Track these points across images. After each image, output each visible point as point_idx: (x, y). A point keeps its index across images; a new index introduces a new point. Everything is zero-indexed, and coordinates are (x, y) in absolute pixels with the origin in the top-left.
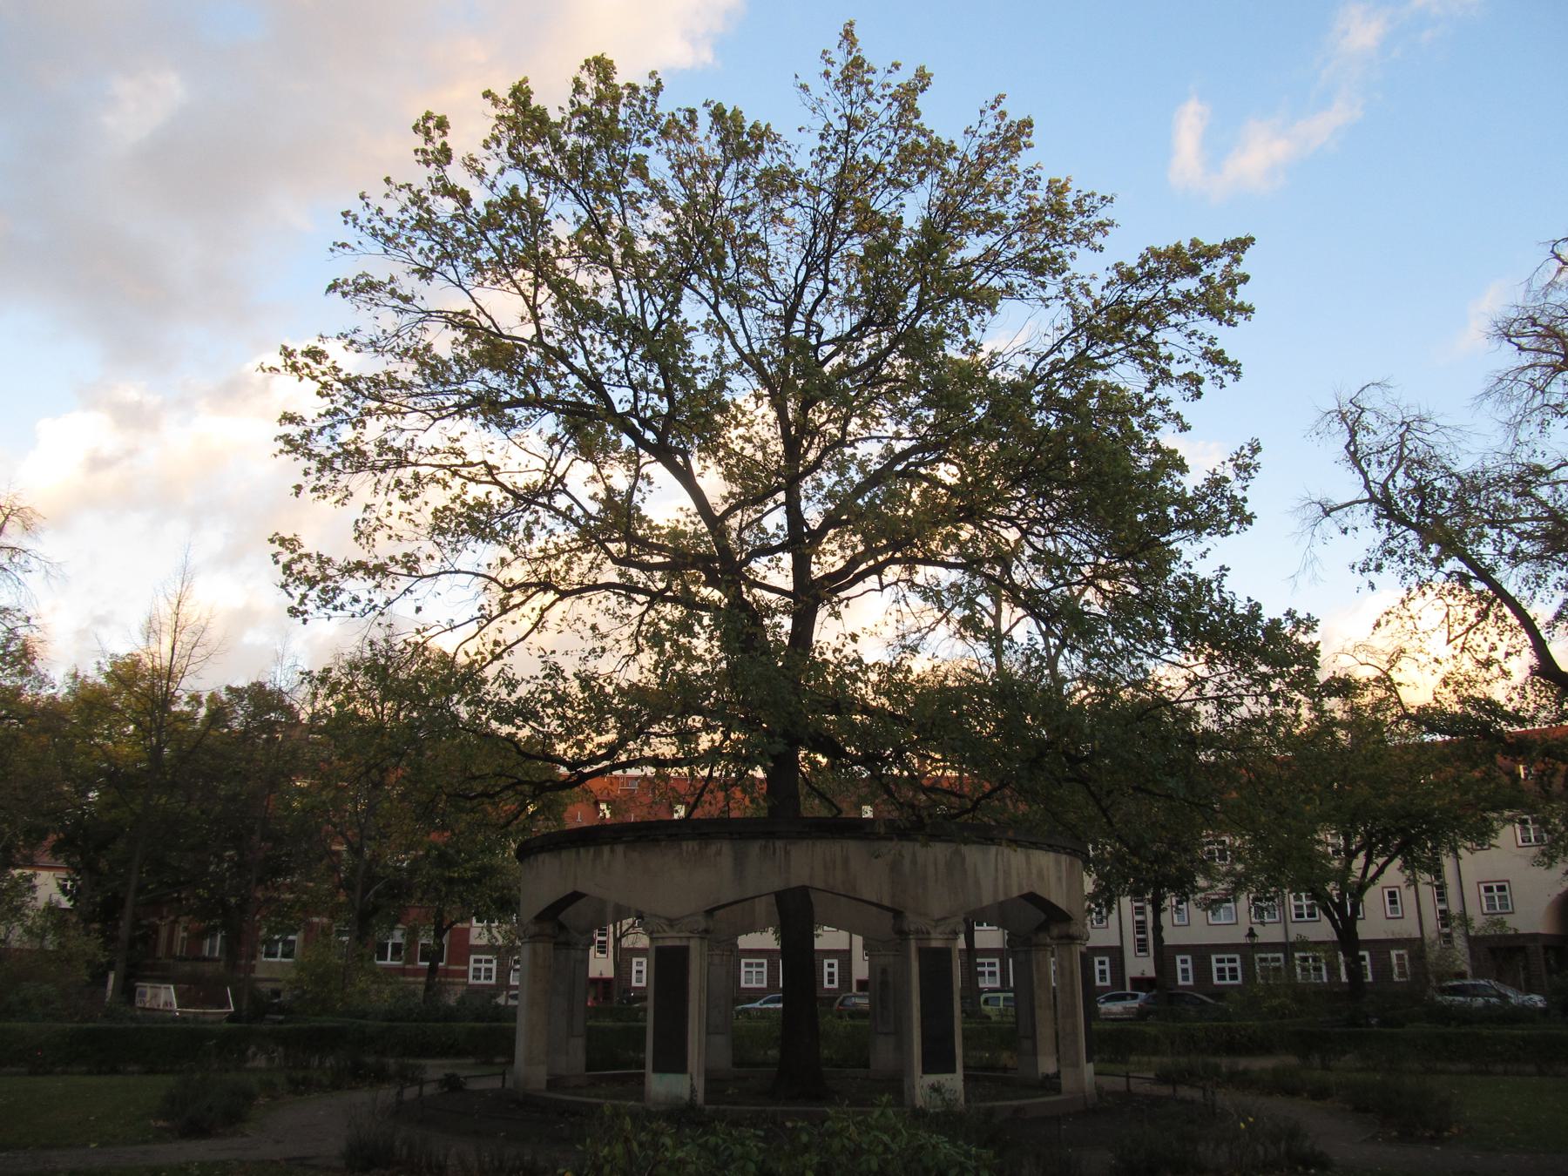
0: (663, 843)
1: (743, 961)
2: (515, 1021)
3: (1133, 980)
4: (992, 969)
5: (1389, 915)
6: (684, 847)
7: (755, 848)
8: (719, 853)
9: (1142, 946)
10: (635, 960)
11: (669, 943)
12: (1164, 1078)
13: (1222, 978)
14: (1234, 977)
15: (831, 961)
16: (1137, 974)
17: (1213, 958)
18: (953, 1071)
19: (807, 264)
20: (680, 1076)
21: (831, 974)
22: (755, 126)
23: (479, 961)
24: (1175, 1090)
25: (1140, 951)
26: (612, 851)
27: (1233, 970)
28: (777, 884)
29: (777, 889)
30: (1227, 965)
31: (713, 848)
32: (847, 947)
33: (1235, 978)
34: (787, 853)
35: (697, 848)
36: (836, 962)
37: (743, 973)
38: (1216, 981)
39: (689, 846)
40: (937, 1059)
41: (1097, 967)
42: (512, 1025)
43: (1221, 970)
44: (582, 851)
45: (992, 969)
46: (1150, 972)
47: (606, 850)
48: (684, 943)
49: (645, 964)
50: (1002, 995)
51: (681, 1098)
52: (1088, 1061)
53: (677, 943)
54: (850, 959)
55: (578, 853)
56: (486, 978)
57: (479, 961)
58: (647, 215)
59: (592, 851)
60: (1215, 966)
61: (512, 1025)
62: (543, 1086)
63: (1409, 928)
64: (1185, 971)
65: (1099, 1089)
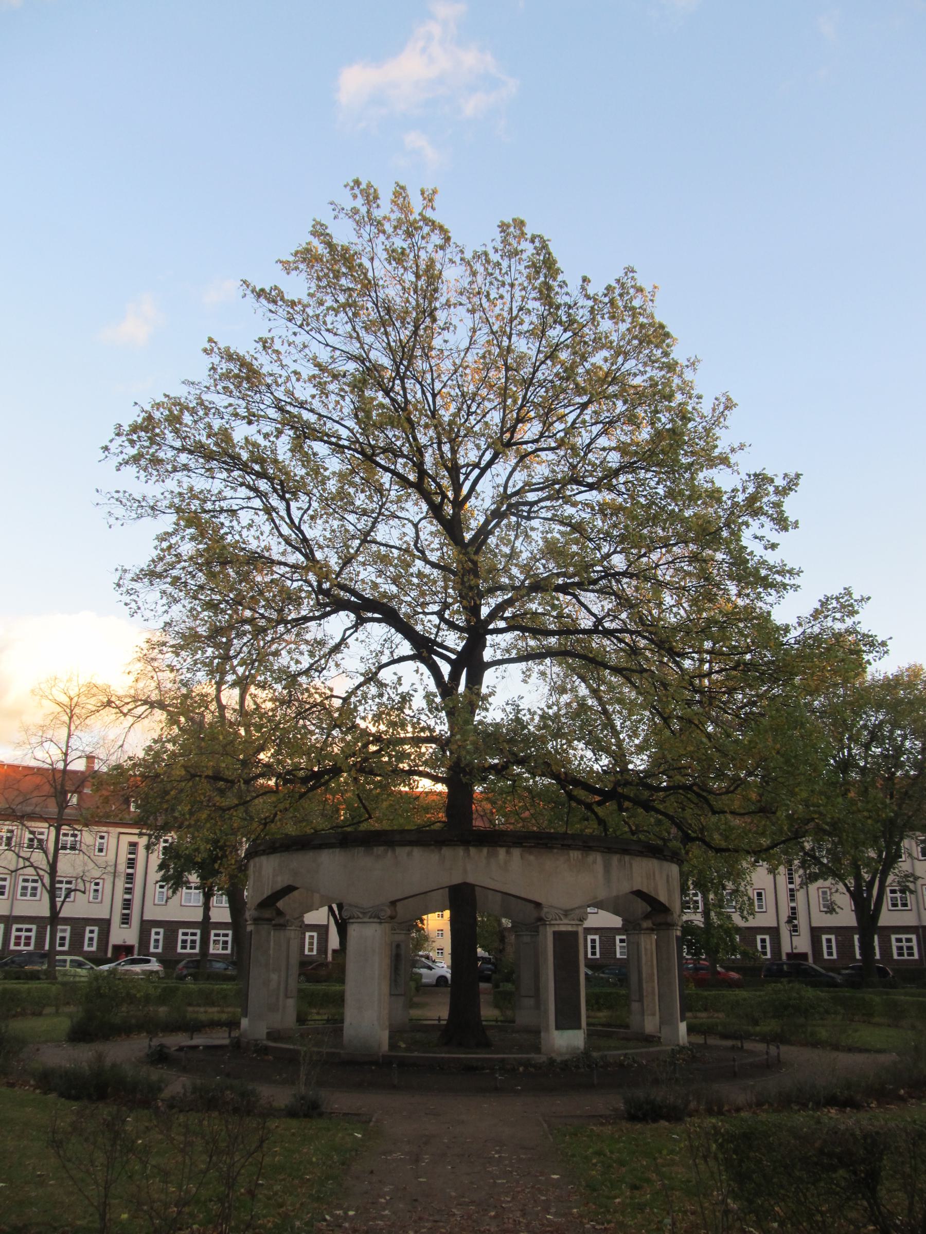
0: (555, 851)
1: (213, 932)
4: (225, 939)
6: (572, 855)
7: (615, 859)
8: (595, 862)
9: (126, 919)
10: (154, 931)
11: (563, 928)
14: (225, 948)
15: (92, 928)
17: (181, 931)
20: (576, 1032)
22: (501, 232)
24: (705, 1039)
25: (123, 923)
26: (508, 852)
27: (193, 942)
28: (456, 880)
31: (590, 858)
32: (108, 917)
33: (193, 948)
34: (631, 864)
35: (580, 857)
36: (96, 929)
37: (212, 942)
38: (179, 950)
39: (575, 855)
40: (568, 1019)
41: (153, 937)
42: (337, 988)
43: (184, 941)
44: (473, 850)
45: (225, 939)
47: (502, 852)
48: (574, 929)
49: (230, 936)
50: (69, 958)
51: (578, 1048)
52: (682, 1021)
53: (570, 928)
55: (468, 851)
58: (461, 294)
59: (485, 850)
60: (181, 937)
61: (337, 988)
62: (265, 1036)
64: (157, 941)
65: (690, 1043)
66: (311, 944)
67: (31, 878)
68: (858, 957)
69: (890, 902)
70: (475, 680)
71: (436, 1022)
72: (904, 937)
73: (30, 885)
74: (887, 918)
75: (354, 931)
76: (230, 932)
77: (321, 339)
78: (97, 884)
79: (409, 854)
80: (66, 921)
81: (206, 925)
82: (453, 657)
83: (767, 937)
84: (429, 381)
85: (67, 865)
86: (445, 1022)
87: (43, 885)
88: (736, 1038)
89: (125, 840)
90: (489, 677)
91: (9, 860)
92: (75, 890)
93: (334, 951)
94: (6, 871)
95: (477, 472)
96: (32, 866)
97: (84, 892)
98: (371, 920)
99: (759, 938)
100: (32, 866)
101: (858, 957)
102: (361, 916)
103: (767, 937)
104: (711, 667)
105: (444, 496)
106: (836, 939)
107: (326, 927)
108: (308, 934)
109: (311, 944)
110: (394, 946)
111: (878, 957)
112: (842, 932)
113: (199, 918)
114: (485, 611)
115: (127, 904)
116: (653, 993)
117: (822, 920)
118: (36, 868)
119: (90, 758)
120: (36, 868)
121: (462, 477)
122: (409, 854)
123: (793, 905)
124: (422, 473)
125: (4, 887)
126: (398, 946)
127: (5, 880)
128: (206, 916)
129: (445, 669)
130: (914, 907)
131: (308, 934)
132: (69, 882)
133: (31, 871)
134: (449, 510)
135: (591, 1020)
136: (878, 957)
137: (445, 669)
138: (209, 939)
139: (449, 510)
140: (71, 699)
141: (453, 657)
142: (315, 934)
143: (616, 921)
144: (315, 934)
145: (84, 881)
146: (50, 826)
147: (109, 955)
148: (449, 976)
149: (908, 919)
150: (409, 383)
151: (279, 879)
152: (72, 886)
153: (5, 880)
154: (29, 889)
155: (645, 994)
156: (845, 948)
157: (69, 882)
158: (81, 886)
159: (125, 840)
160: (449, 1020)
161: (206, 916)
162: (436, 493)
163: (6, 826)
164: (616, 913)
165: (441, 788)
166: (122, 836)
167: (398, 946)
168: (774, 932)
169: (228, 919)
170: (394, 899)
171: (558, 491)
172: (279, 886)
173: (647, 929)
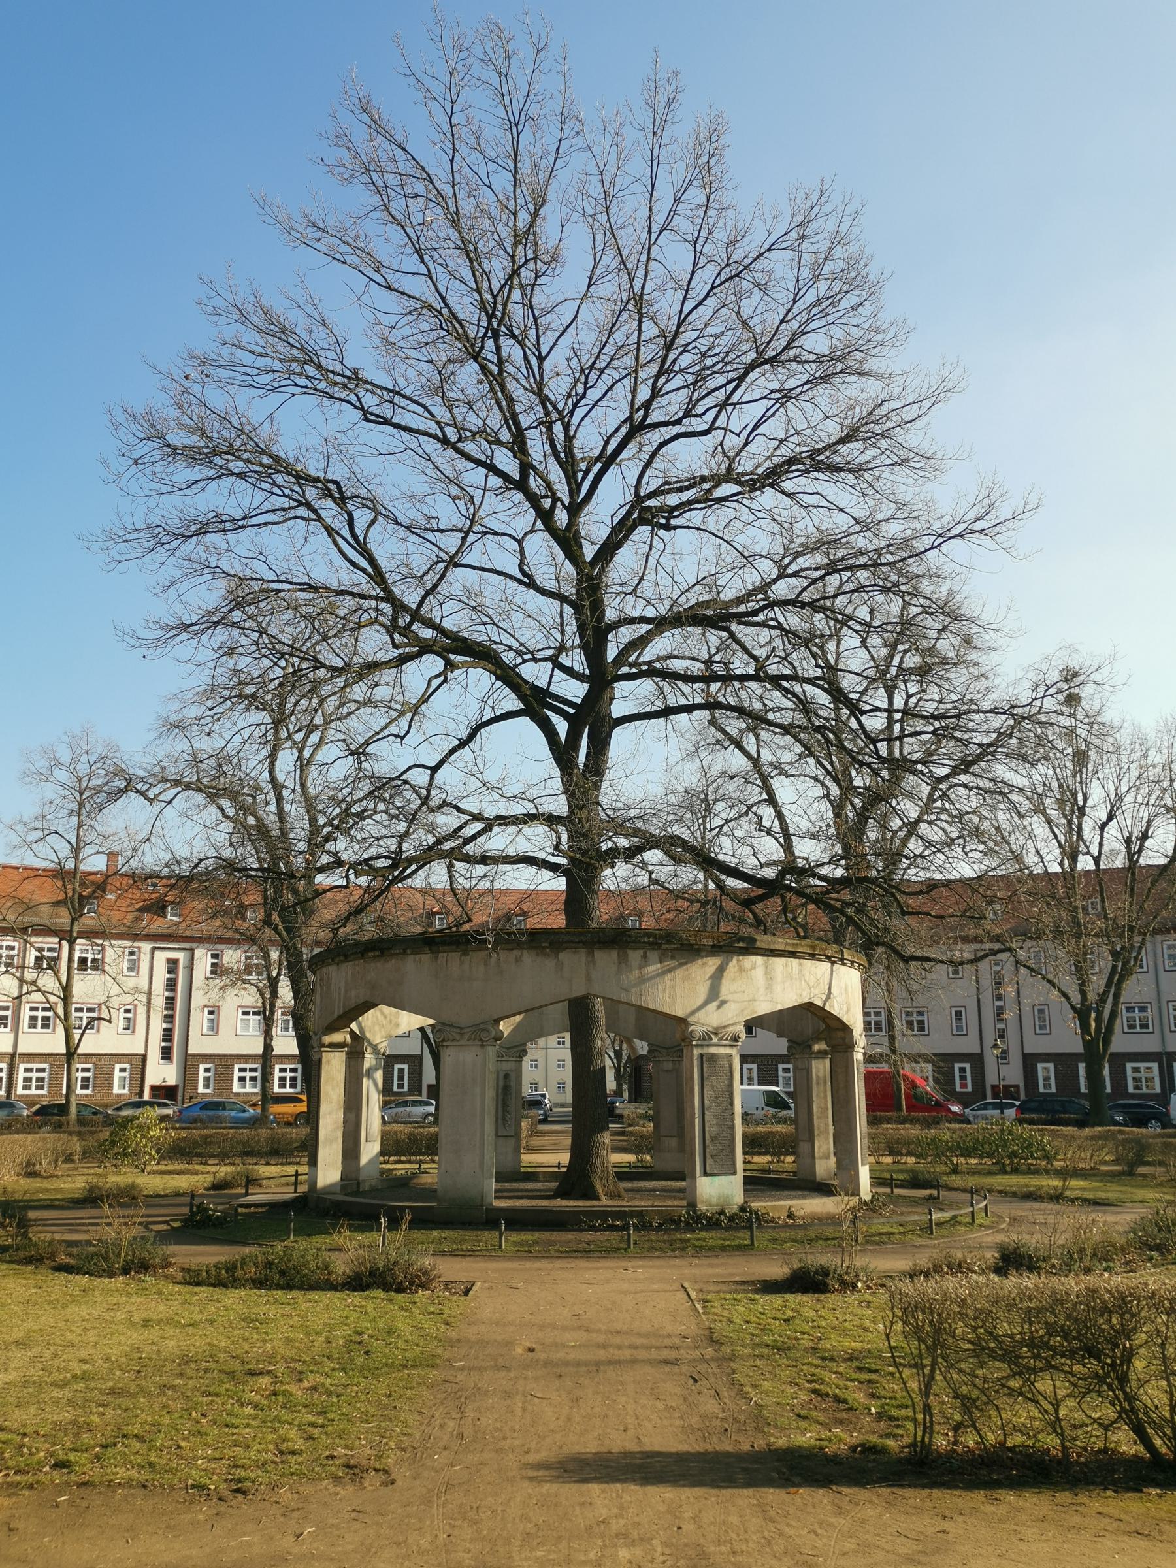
2: (869, 1134)
3: (154, 1088)
5: (955, 1032)
9: (166, 1054)
12: (251, 1181)
13: (283, 1086)
14: (293, 1086)
16: (158, 1082)
18: (734, 1173)
19: (668, 519)
21: (1047, 1079)
23: (284, 1070)
27: (293, 1079)
29: (574, 995)
30: (34, 1075)
32: (979, 1051)
45: (254, 1074)
46: (172, 1081)
49: (300, 1071)
52: (863, 1164)
54: (982, 1062)
56: (37, 1088)
57: (284, 1070)
60: (237, 1074)
63: (969, 1045)
64: (207, 1079)
66: (401, 1079)
67: (41, 1006)
68: (1083, 1090)
69: (1125, 1023)
70: (600, 746)
71: (556, 1169)
72: (1142, 1065)
73: (40, 1014)
74: (1120, 1043)
75: (449, 1056)
76: (299, 1067)
77: (381, 280)
78: (128, 1011)
79: (518, 960)
80: (88, 1056)
81: (267, 1057)
82: (572, 711)
83: (967, 1066)
84: (534, 340)
85: (86, 987)
86: (565, 1169)
87: (56, 1015)
88: (932, 1187)
89: (161, 957)
90: (620, 739)
91: (9, 984)
92: (100, 1019)
93: (429, 1086)
94: (5, 998)
95: (599, 465)
96: (39, 990)
97: (110, 1021)
98: (471, 1042)
99: (957, 1066)
100: (39, 990)
101: (1083, 1090)
102: (458, 1037)
103: (967, 1066)
104: (902, 729)
105: (555, 499)
106: (1055, 1068)
107: (420, 1058)
108: (396, 1067)
109: (401, 1079)
110: (502, 1075)
111: (1108, 1090)
112: (1064, 1062)
113: (259, 1049)
114: (611, 653)
115: (168, 1035)
116: (827, 1131)
117: (1035, 1045)
118: (44, 993)
119: (112, 855)
120: (44, 993)
121: (580, 475)
122: (518, 960)
123: (1001, 1026)
124: (526, 467)
125: (6, 1018)
126: (506, 1076)
127: (7, 1008)
128: (268, 1047)
129: (562, 727)
130: (1157, 1030)
131: (396, 1067)
132: (89, 1010)
133: (37, 997)
134: (561, 518)
135: (749, 1167)
136: (1108, 1090)
137: (562, 727)
138: (272, 1074)
139: (561, 518)
140: (80, 780)
141: (572, 711)
142: (406, 1067)
143: (781, 1046)
144: (406, 1067)
145: (108, 1008)
146: (61, 939)
147: (147, 1096)
148: (506, 1034)
149: (1149, 1043)
150: (507, 344)
151: (353, 993)
152: (95, 1015)
153: (7, 1008)
154: (40, 1019)
155: (816, 1132)
156: (1066, 1076)
157: (89, 1010)
158: (105, 1015)
159: (161, 957)
160: (570, 1166)
161: (268, 1047)
162: (546, 497)
163: (9, 941)
164: (780, 1035)
165: (560, 883)
166: (157, 953)
167: (506, 1076)
168: (977, 1060)
169: (295, 1051)
170: (496, 1017)
171: (709, 491)
172: (353, 1003)
173: (819, 1052)
